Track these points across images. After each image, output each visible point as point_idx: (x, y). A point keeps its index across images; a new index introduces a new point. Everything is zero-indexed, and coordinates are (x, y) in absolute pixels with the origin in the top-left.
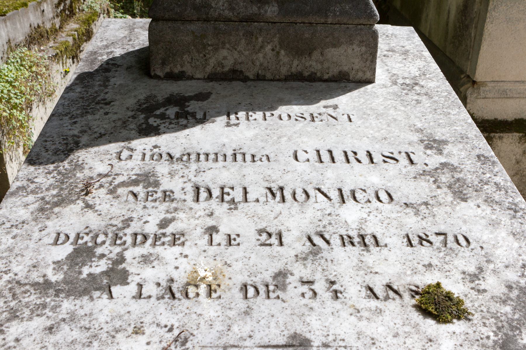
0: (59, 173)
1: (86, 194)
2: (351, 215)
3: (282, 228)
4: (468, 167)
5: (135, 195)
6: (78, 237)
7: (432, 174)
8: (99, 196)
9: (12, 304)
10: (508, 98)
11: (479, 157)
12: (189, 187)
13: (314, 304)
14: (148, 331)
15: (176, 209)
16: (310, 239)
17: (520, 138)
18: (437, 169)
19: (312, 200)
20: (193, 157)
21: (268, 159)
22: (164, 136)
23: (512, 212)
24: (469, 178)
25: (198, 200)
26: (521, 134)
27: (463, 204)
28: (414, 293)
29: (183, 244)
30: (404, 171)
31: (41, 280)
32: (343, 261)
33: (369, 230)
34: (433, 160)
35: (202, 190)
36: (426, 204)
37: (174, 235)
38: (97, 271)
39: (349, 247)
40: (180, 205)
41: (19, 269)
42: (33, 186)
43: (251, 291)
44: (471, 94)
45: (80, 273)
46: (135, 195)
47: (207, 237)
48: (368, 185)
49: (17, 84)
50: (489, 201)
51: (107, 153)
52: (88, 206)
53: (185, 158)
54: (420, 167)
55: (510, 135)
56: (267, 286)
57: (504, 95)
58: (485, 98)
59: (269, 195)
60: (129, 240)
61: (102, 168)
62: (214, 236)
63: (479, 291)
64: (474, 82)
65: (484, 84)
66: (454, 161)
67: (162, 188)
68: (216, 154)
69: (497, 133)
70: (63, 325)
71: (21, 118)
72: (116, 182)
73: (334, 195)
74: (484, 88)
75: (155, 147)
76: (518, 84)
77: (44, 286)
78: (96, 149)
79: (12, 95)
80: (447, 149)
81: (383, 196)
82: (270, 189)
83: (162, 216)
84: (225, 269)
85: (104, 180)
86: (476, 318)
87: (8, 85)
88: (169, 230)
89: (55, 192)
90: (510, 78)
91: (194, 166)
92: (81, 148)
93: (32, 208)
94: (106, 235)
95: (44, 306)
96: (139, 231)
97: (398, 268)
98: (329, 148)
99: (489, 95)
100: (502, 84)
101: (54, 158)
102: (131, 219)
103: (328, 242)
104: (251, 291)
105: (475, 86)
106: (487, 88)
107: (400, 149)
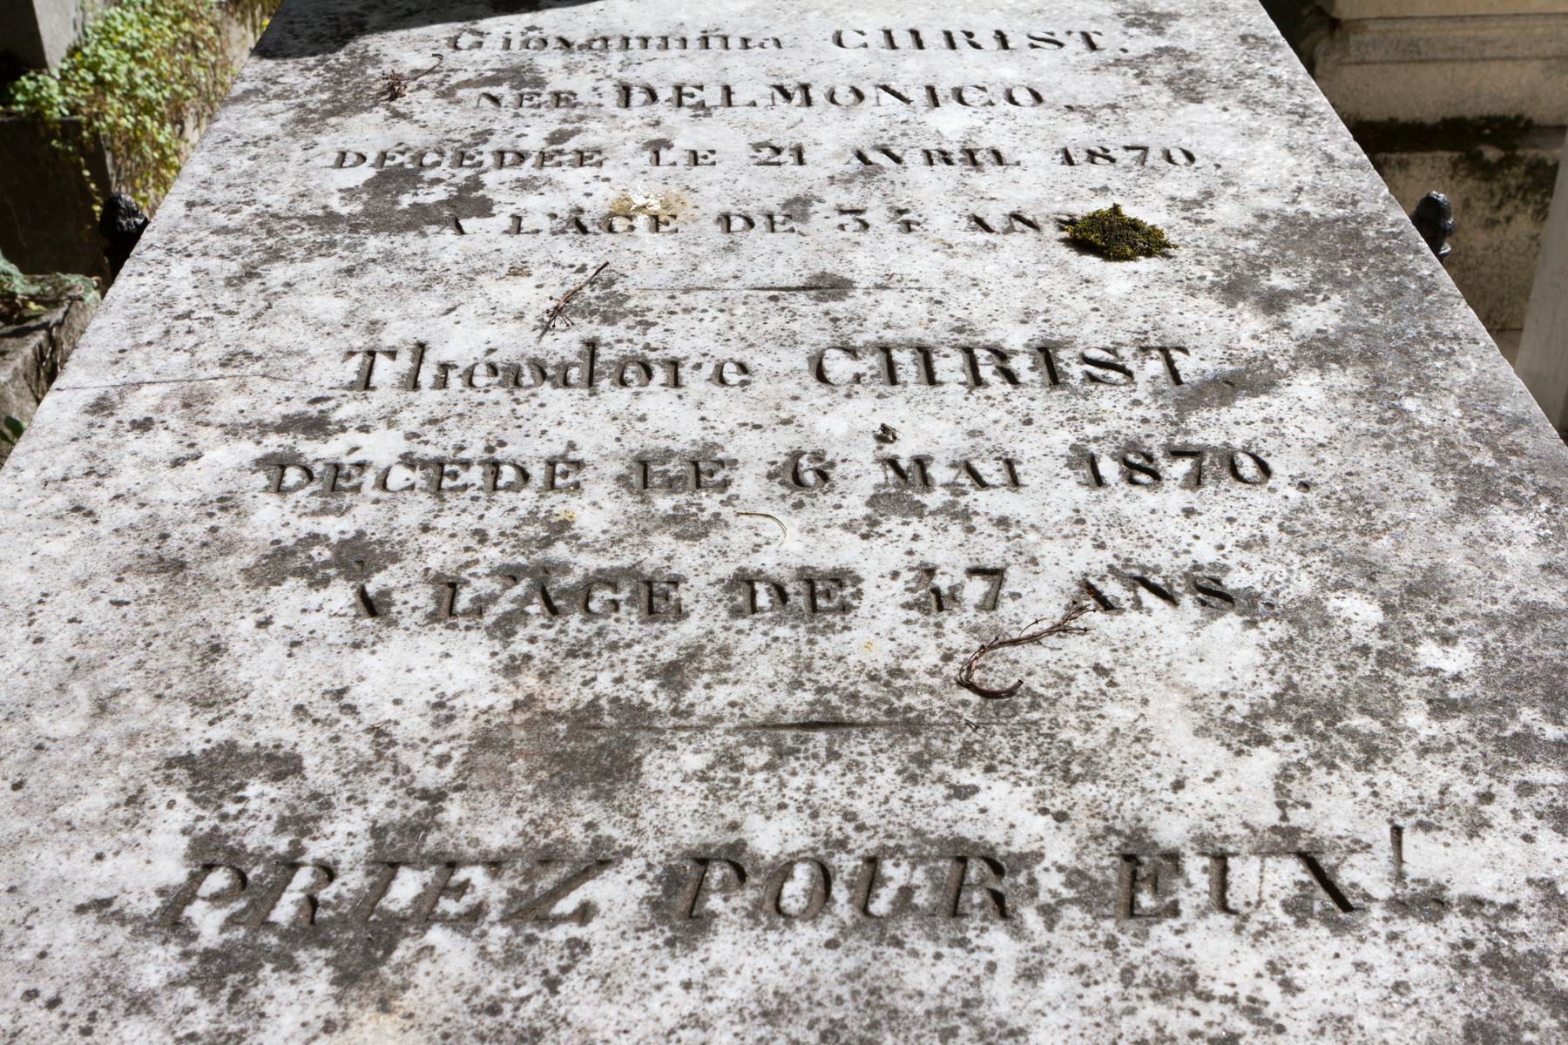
0: (329, 69)
1: (392, 98)
2: (951, 124)
3: (804, 142)
4: (1217, 54)
5: (495, 100)
6: (383, 156)
7: (1140, 67)
8: (421, 102)
9: (269, 242)
10: (1422, 61)
11: (1244, 38)
12: (608, 87)
13: (863, 238)
14: (536, 273)
15: (581, 118)
16: (860, 156)
17: (1455, 165)
18: (1145, 57)
19: (869, 102)
20: (615, 43)
21: (778, 43)
22: (549, 13)
23: (1296, 118)
24: (1214, 69)
25: (627, 105)
26: (1456, 155)
27: (1193, 106)
28: (1062, 225)
29: (600, 164)
30: (1073, 60)
31: (320, 213)
32: (929, 189)
33: (985, 142)
34: (1140, 43)
35: (635, 91)
36: (1113, 107)
37: (580, 153)
38: (431, 200)
39: (940, 167)
40: (589, 111)
41: (276, 199)
42: (276, 89)
43: (738, 224)
44: (1326, 54)
45: (396, 203)
46: (495, 100)
47: (648, 154)
48: (991, 80)
49: (147, 54)
50: (1249, 101)
51: (428, 38)
52: (396, 114)
53: (597, 45)
54: (1108, 55)
55: (1428, 156)
56: (770, 216)
57: (1413, 54)
58: (1362, 62)
59: (778, 96)
60: (489, 160)
61: (424, 61)
62: (663, 153)
63: (1197, 222)
64: (1335, 24)
65: (1358, 25)
66: (1188, 45)
67: (549, 88)
68: (665, 39)
69: (1392, 151)
70: (371, 266)
71: (161, 139)
72: (453, 81)
73: (918, 95)
74: (1359, 38)
75: (532, 28)
76: (1448, 25)
77: (330, 219)
78: (404, 33)
79: (138, 80)
80: (1173, 28)
81: (1022, 96)
82: (781, 89)
83: (555, 127)
84: (685, 196)
85: (425, 78)
86: (1182, 254)
87: (127, 57)
88: (571, 145)
89: (325, 96)
90: (1427, 7)
91: (616, 57)
92: (371, 32)
93: (281, 118)
94: (441, 154)
95: (332, 244)
96: (508, 147)
97: (1039, 192)
98: (912, 26)
99: (1374, 55)
100: (1404, 25)
101: (313, 48)
102: (491, 132)
103: (897, 160)
104: (738, 224)
105: (1338, 34)
106: (1367, 38)
107: (1069, 27)
